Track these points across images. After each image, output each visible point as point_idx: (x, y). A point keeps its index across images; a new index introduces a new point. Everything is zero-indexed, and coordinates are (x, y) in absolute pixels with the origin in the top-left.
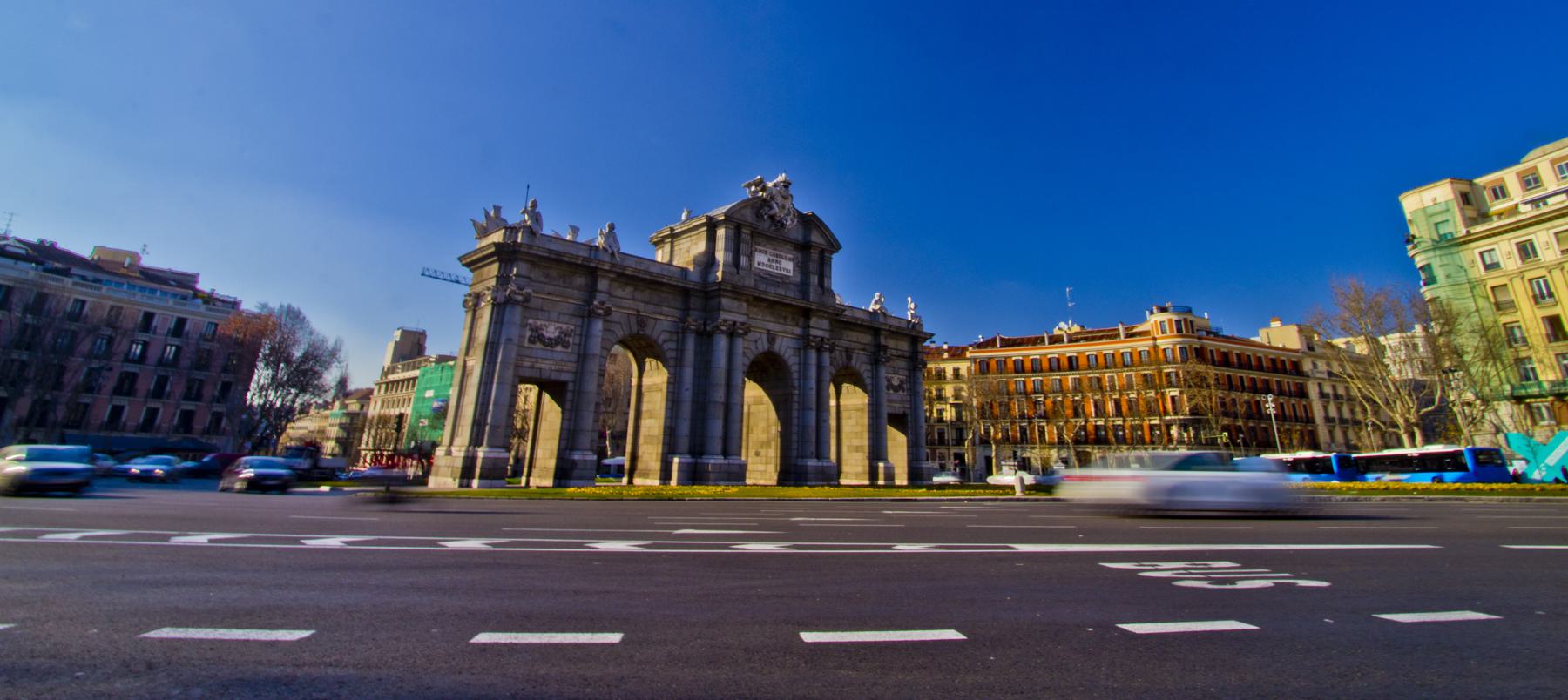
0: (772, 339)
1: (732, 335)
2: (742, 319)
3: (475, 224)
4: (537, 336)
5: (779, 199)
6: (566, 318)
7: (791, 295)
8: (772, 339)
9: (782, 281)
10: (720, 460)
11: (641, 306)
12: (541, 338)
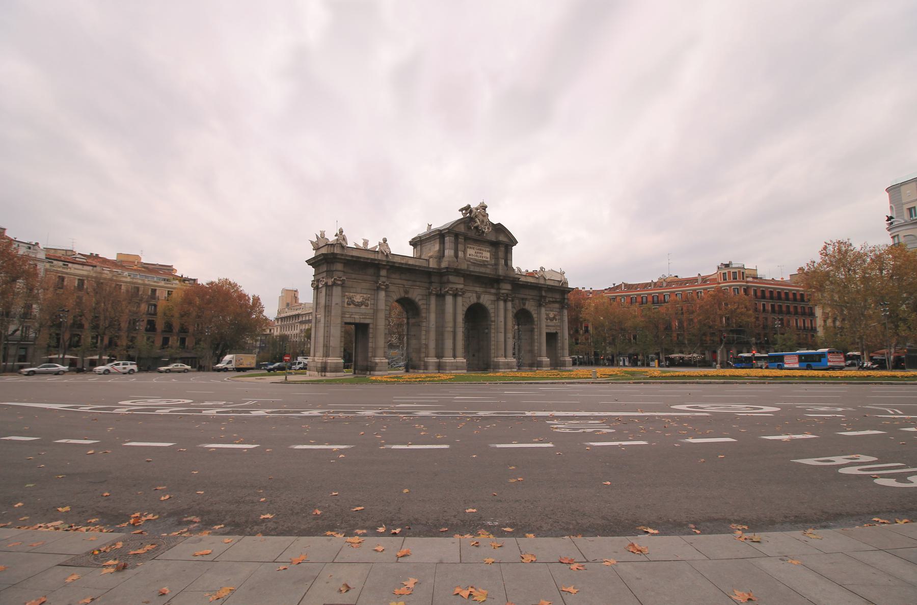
0: (479, 298)
1: (455, 296)
2: (461, 286)
3: (312, 242)
4: (352, 302)
5: (481, 217)
6: (364, 291)
7: (488, 271)
8: (479, 298)
9: (484, 264)
10: (452, 360)
11: (405, 283)
12: (353, 302)
